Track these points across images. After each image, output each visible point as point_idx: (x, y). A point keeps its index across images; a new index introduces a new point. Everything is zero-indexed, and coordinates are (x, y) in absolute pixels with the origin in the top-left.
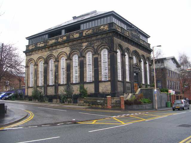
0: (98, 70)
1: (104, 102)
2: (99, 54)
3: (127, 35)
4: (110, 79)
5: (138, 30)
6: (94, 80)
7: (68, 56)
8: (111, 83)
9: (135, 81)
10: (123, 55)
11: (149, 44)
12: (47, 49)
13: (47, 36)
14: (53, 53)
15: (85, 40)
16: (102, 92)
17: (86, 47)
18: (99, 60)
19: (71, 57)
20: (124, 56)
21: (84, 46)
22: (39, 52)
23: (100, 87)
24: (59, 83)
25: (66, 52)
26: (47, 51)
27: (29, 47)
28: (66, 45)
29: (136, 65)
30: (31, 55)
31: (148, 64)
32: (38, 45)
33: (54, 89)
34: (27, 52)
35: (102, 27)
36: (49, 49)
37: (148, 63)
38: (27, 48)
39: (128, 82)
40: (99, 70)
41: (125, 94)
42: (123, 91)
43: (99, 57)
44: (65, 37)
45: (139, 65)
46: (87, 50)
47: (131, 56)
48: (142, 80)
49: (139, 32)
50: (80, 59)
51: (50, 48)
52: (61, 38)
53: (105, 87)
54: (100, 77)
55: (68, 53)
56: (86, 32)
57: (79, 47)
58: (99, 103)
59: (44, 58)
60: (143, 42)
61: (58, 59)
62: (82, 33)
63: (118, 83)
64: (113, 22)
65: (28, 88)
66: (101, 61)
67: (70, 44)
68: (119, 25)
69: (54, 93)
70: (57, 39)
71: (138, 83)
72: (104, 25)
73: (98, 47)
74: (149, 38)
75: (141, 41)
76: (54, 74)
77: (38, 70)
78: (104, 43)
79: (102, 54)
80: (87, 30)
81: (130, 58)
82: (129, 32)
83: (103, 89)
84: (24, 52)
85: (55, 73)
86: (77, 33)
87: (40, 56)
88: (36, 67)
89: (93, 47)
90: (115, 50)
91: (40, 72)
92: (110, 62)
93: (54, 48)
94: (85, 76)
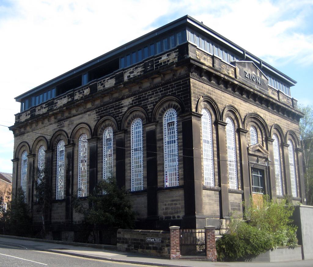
1: (162, 242)
2: (158, 122)
3: (231, 75)
5: (262, 65)
7: (93, 131)
9: (257, 190)
10: (218, 123)
11: (292, 99)
13: (54, 91)
14: (63, 127)
16: (164, 216)
17: (129, 109)
18: (158, 136)
21: (126, 106)
23: (159, 204)
25: (89, 123)
28: (89, 106)
29: (258, 148)
32: (37, 110)
35: (164, 58)
37: (291, 146)
38: (16, 119)
40: (158, 162)
43: (158, 130)
44: (87, 90)
45: (265, 148)
46: (131, 116)
49: (264, 70)
52: (80, 93)
53: (172, 204)
54: (159, 179)
55: (93, 124)
56: (131, 73)
58: (152, 243)
59: (46, 139)
62: (122, 75)
63: (205, 192)
66: (162, 139)
70: (72, 96)
72: (169, 54)
73: (154, 106)
74: (293, 85)
78: (169, 95)
79: (164, 123)
80: (131, 69)
81: (239, 132)
83: (166, 209)
87: (39, 135)
89: (145, 107)
90: (194, 110)
92: (182, 141)
94: (127, 178)
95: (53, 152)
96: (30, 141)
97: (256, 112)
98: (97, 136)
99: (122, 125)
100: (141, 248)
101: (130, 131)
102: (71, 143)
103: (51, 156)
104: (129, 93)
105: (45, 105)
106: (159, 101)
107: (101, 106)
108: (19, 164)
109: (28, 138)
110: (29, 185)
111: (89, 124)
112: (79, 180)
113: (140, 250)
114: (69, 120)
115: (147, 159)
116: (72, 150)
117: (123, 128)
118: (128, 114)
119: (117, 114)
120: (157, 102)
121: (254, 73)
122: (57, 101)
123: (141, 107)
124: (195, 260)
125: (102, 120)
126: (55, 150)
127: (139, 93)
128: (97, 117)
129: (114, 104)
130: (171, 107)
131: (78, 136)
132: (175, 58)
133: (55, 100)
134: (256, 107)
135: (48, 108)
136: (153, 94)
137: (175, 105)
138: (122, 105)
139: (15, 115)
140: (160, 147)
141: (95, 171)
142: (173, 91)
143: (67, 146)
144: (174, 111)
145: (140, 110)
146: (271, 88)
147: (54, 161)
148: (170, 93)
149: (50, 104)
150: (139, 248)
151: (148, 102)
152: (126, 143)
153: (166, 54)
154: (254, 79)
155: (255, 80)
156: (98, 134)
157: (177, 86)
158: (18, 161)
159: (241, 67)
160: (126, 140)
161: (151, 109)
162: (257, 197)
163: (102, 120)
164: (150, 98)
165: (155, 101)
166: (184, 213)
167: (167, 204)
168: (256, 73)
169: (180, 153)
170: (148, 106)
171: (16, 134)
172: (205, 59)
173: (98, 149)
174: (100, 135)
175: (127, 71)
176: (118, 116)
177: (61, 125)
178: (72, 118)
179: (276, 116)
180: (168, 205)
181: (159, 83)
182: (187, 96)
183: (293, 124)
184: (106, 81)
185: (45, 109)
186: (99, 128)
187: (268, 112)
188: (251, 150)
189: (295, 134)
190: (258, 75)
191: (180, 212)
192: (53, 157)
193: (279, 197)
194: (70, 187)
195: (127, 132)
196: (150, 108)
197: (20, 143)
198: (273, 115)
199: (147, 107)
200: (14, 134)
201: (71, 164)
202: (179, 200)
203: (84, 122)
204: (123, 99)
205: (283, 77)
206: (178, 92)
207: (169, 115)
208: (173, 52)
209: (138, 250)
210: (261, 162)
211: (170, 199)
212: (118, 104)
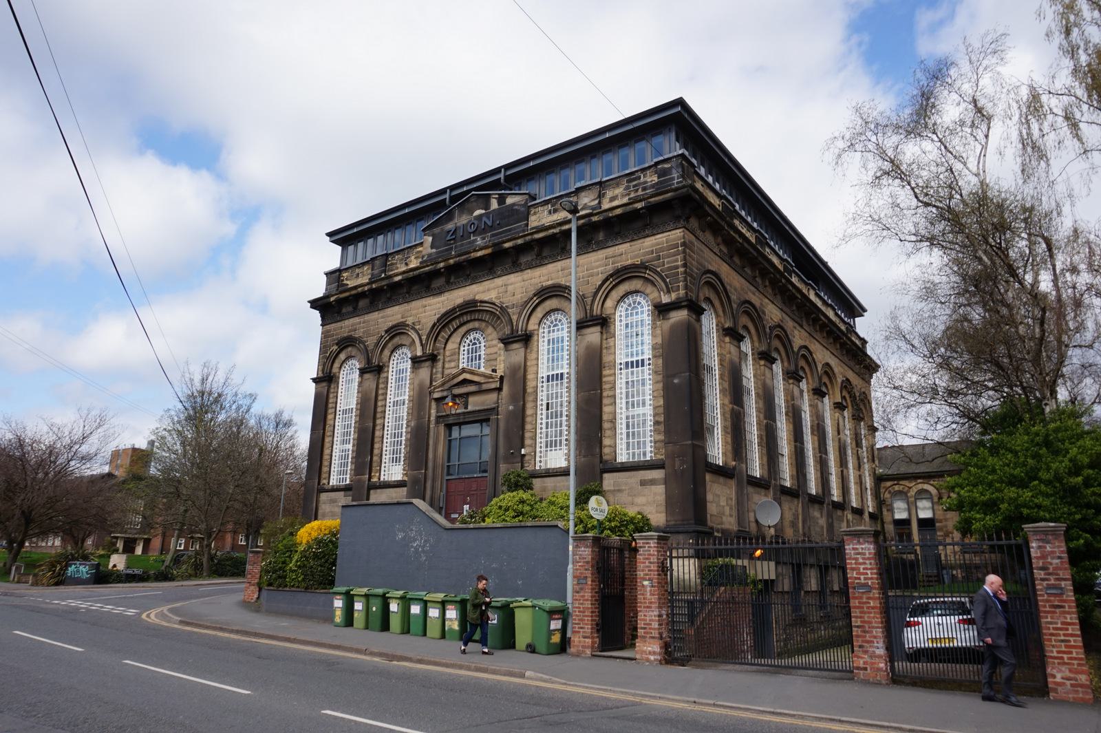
117: (599, 312)
139: (326, 274)
144: (622, 307)
169: (610, 375)
207: (471, 341)
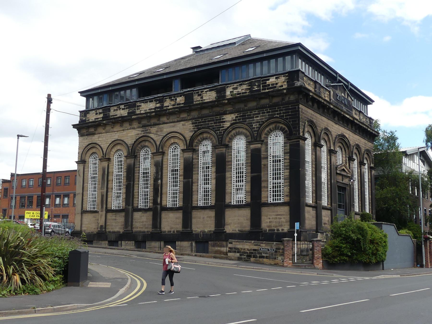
0: (259, 177)
2: (263, 141)
3: (326, 98)
4: (287, 199)
5: (350, 86)
6: (249, 200)
7: (188, 142)
8: (291, 211)
10: (316, 145)
12: (135, 124)
14: (150, 133)
15: (229, 109)
16: (268, 229)
17: (232, 124)
18: (263, 154)
19: (196, 146)
20: (318, 148)
21: (228, 121)
22: (115, 129)
24: (164, 203)
25: (182, 133)
26: (136, 127)
27: (88, 116)
28: (184, 115)
29: (344, 167)
30: (93, 134)
31: (324, 149)
32: (112, 111)
33: (151, 218)
34: (83, 128)
35: (272, 80)
36: (139, 123)
37: (367, 165)
39: (325, 208)
40: (262, 179)
41: (319, 234)
42: (315, 228)
43: (263, 149)
44: (181, 98)
46: (234, 132)
47: (332, 148)
48: (354, 202)
49: (351, 91)
50: (218, 151)
51: (144, 122)
52: (172, 100)
55: (188, 135)
56: (234, 89)
57: (216, 123)
60: (358, 113)
61: (162, 149)
63: (307, 209)
64: (299, 70)
65: (82, 213)
67: (195, 114)
68: (310, 76)
69: (151, 226)
70: (161, 101)
71: (346, 209)
72: (277, 76)
73: (261, 125)
75: (354, 112)
76: (151, 182)
77: (110, 170)
80: (235, 86)
81: (331, 152)
82: (330, 92)
83: (270, 222)
84: (74, 126)
85: (156, 180)
86: (210, 91)
88: (105, 164)
89: (250, 125)
90: (301, 134)
91: (114, 178)
93: (153, 121)
95: (135, 158)
96: (103, 143)
97: (343, 133)
98: (193, 147)
99: (224, 139)
100: (253, 257)
101: (231, 147)
102: (160, 151)
103: (133, 162)
104: (232, 109)
105: (123, 106)
106: (266, 121)
107: (199, 118)
108: (86, 167)
109: (100, 139)
110: (102, 191)
111: (183, 134)
112: (168, 190)
113: (252, 259)
114: (157, 126)
115: (251, 175)
116: (161, 158)
118: (230, 129)
119: (217, 128)
120: (264, 122)
121: (343, 94)
122: (140, 104)
123: (246, 125)
124: (305, 268)
125: (200, 131)
126: (138, 156)
127: (243, 111)
128: (193, 128)
129: (214, 117)
130: (278, 129)
131: (169, 145)
132: (284, 82)
133: (138, 103)
134: (344, 129)
135: (129, 110)
136: (260, 114)
137: (282, 127)
138: (224, 120)
140: (265, 165)
141: (191, 181)
142: (281, 113)
143: (154, 154)
145: (244, 127)
146: (355, 108)
147: (136, 168)
148: (278, 116)
149: (131, 105)
150: (251, 257)
151: (253, 120)
152: (226, 157)
153: (275, 77)
154: (343, 101)
155: (343, 102)
156: (194, 146)
157: (285, 110)
158: (85, 163)
159: (334, 90)
160: (227, 154)
161: (257, 128)
162: (340, 214)
163: (200, 131)
164: (256, 117)
165: (261, 121)
166: (289, 227)
167: (271, 218)
168: (345, 95)
170: (254, 125)
171: (81, 132)
172: (309, 84)
173: (194, 161)
174: (195, 147)
175: (230, 86)
176: (219, 130)
177: (147, 130)
178: (161, 125)
179: (357, 136)
180: (272, 218)
181: (267, 104)
182: (296, 121)
183: (370, 143)
184: (204, 92)
185: (123, 111)
186: (195, 139)
187: (352, 133)
188: (338, 169)
189: (370, 153)
190: (346, 97)
191: (284, 225)
192: (136, 164)
193: (356, 214)
194: (158, 196)
195: (228, 147)
196: (256, 126)
197: (88, 143)
198: (355, 135)
199: (253, 126)
200: (79, 133)
201: (160, 173)
202: (284, 215)
203: (176, 131)
204: (225, 113)
205: (365, 97)
206: (286, 116)
208: (282, 76)
209: (251, 259)
210: (346, 181)
211: (274, 214)
212: (219, 118)
